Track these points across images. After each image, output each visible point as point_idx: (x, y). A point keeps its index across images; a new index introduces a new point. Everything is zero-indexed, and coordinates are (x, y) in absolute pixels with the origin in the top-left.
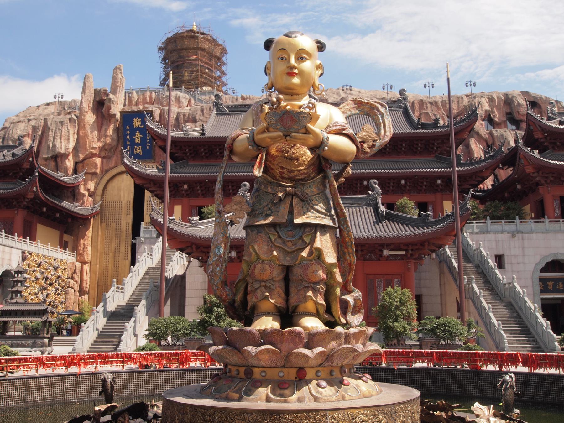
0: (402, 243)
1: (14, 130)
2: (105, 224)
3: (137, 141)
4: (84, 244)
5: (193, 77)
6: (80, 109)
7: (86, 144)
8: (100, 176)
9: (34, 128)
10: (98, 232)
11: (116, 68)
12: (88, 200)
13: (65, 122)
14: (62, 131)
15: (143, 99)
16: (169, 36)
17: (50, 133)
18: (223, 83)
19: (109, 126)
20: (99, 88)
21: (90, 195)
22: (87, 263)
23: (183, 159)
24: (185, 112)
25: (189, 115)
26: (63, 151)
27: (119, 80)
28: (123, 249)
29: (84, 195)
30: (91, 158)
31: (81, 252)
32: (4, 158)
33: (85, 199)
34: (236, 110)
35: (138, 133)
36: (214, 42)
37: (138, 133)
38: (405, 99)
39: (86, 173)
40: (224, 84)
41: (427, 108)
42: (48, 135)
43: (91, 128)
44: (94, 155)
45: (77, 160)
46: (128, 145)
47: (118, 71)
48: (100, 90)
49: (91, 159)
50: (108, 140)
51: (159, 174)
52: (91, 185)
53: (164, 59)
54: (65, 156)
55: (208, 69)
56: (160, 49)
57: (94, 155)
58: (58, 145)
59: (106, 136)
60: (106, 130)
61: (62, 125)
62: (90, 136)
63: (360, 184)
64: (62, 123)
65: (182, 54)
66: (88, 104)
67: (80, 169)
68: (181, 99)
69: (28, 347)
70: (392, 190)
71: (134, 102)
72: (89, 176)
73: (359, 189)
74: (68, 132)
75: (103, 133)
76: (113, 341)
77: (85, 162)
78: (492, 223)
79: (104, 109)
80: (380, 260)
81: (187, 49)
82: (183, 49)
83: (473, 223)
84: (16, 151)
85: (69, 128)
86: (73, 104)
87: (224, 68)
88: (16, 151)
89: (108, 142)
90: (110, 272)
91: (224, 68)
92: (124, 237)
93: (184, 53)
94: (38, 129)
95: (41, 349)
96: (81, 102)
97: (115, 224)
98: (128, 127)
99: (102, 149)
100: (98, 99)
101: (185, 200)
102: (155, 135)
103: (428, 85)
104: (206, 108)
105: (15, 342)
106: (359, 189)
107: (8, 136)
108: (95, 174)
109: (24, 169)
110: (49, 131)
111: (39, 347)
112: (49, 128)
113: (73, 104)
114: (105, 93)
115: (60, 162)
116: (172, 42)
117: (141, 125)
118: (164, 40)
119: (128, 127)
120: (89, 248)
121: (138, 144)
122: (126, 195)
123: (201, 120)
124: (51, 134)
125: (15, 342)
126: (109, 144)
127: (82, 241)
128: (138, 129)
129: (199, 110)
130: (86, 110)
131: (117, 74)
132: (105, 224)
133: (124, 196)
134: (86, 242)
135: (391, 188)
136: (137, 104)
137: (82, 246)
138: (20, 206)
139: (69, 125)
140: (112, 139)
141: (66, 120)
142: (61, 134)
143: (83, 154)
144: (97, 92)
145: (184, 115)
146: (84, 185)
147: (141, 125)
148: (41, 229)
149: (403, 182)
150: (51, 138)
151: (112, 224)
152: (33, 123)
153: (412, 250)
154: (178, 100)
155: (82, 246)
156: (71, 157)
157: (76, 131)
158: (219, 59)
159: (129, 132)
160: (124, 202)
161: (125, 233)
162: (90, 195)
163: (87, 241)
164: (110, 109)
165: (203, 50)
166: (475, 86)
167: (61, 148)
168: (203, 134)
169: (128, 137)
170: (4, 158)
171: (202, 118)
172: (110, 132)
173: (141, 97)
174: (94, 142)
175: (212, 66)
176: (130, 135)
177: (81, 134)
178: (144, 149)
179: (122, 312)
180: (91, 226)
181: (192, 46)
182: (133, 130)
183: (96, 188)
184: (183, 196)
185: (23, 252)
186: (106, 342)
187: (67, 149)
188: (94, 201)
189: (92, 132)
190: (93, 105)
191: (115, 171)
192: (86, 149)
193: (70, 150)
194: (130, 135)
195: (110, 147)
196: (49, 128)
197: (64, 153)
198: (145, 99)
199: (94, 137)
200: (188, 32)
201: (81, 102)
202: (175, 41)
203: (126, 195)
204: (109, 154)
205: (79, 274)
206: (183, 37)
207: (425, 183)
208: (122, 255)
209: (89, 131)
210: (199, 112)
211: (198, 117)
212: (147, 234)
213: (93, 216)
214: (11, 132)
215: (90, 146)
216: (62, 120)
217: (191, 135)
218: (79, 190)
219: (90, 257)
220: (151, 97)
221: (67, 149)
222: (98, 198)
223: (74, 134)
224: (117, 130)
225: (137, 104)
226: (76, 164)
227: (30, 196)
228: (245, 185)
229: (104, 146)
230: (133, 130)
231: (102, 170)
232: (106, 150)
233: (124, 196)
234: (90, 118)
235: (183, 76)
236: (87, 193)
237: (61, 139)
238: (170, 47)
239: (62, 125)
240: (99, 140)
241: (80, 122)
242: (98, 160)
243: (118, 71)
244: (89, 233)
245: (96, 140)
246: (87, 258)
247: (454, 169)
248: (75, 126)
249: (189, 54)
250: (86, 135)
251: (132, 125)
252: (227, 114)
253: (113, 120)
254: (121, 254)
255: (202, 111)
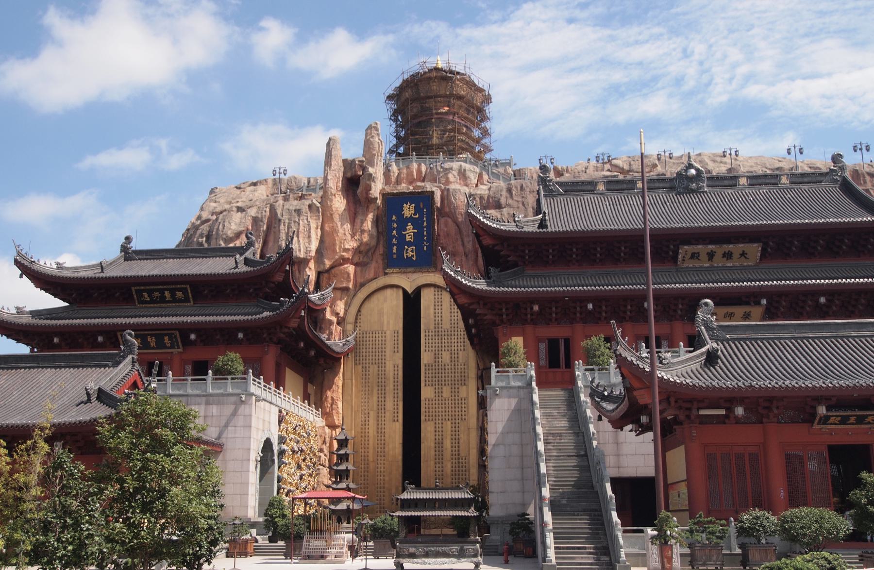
0: (761, 397)
1: (226, 224)
2: (360, 367)
3: (408, 238)
4: (332, 398)
5: (445, 139)
6: (324, 187)
7: (334, 245)
8: (352, 293)
9: (256, 221)
10: (352, 380)
11: (370, 127)
12: (336, 329)
13: (304, 210)
14: (299, 224)
15: (407, 174)
16: (406, 77)
17: (282, 227)
18: (484, 146)
19: (367, 215)
20: (350, 158)
21: (338, 323)
22: (338, 427)
23: (516, 265)
24: (483, 192)
25: (489, 197)
26: (302, 255)
27: (376, 145)
28: (390, 405)
29: (331, 322)
30: (341, 265)
31: (328, 410)
32: (102, 271)
33: (333, 327)
34: (574, 188)
35: (410, 226)
36: (470, 84)
37: (410, 226)
38: (843, 169)
39: (335, 289)
40: (488, 149)
41: (865, 182)
42: (279, 231)
43: (341, 220)
44: (345, 261)
45: (321, 269)
46: (395, 244)
47: (374, 132)
48: (353, 161)
49: (342, 267)
50: (366, 238)
51: (489, 288)
52: (340, 307)
53: (395, 113)
54: (305, 262)
55: (466, 127)
56: (390, 98)
57: (345, 261)
58: (295, 246)
59: (363, 231)
60: (362, 223)
61: (299, 215)
62: (341, 231)
63: (581, 307)
64: (298, 212)
65: (427, 105)
66: (335, 182)
67: (325, 282)
68: (468, 173)
69: (453, 556)
70: (630, 318)
71: (393, 179)
72: (338, 293)
73: (554, 315)
74: (309, 225)
75: (357, 227)
76: (585, 548)
77: (333, 271)
78: (498, 372)
79: (359, 191)
80: (725, 423)
81: (436, 96)
82: (430, 97)
83: (508, 372)
84: (248, 254)
85: (309, 219)
86: (294, 183)
87: (487, 125)
88: (248, 254)
89: (365, 240)
90: (371, 442)
91: (487, 125)
92: (392, 386)
93: (431, 103)
94: (262, 221)
95: (475, 559)
96: (326, 179)
97: (376, 366)
98: (394, 218)
99: (357, 251)
100: (349, 175)
101: (529, 329)
102: (482, 228)
103: (728, 152)
104: (516, 188)
105: (433, 549)
106: (554, 315)
107: (217, 233)
108: (346, 289)
109: (274, 283)
110: (280, 225)
111: (469, 557)
112: (280, 220)
113: (294, 183)
114: (361, 166)
115: (297, 272)
116: (412, 87)
117: (415, 214)
118: (398, 84)
119: (394, 218)
120: (340, 404)
121: (409, 244)
122: (392, 322)
123: (509, 206)
124: (283, 229)
125: (433, 549)
126: (367, 244)
127: (329, 393)
128: (410, 219)
129: (505, 190)
130: (333, 191)
131: (372, 137)
132: (360, 367)
133: (388, 322)
134: (335, 396)
135: (604, 314)
136: (398, 182)
137: (330, 400)
138: (271, 339)
139: (309, 215)
140: (371, 236)
141: (305, 209)
142: (298, 229)
143: (329, 259)
144: (348, 164)
145: (481, 198)
146: (331, 307)
147: (415, 214)
148: (290, 376)
149: (822, 300)
150: (283, 236)
151: (371, 366)
152: (253, 212)
153: (777, 408)
154: (463, 174)
155: (330, 400)
156: (312, 264)
157: (320, 224)
158: (480, 110)
159: (395, 225)
160: (388, 333)
161: (392, 379)
162: (338, 323)
163: (336, 392)
164: (370, 189)
165: (460, 98)
166: (868, 150)
167: (300, 250)
168: (542, 224)
169: (394, 232)
170: (102, 271)
171: (510, 201)
172: (368, 224)
173: (405, 171)
174: (347, 240)
175: (472, 122)
176: (396, 229)
177: (327, 228)
178: (419, 251)
179: (564, 502)
180: (341, 370)
181: (442, 92)
182: (403, 222)
183: (346, 311)
184: (524, 322)
185: (280, 411)
186: (573, 548)
187: (307, 251)
188: (344, 331)
189: (342, 225)
190: (342, 184)
191: (374, 285)
192: (334, 251)
193: (313, 254)
194: (396, 229)
195: (368, 247)
196: (280, 220)
197: (304, 259)
198: (410, 174)
199: (347, 233)
200: (430, 71)
201: (326, 179)
202: (416, 85)
203: (392, 322)
204: (365, 260)
205: (328, 445)
206: (430, 78)
207: (680, 306)
208: (389, 415)
209: (339, 224)
210: (504, 193)
211: (503, 201)
212: (502, 381)
213: (346, 354)
214: (221, 227)
215: (341, 247)
216: (298, 208)
217: (526, 229)
218: (324, 315)
219: (341, 419)
220: (419, 171)
221: (307, 251)
222: (350, 327)
223: (317, 228)
224: (377, 222)
225: (398, 182)
226: (319, 274)
227: (294, 323)
228: (706, 304)
229: (359, 247)
230: (403, 222)
231: (355, 285)
232: (360, 252)
233: (388, 322)
234: (339, 203)
235: (432, 138)
236: (335, 319)
237: (298, 237)
238: (407, 95)
239: (299, 215)
240: (353, 236)
241: (324, 211)
242: (351, 269)
243: (374, 132)
244: (339, 380)
245: (349, 237)
246: (338, 420)
247: (648, 287)
248: (319, 216)
249: (439, 104)
250: (334, 231)
251: (400, 215)
252: (561, 195)
253: (372, 207)
254: (387, 414)
255: (509, 191)
